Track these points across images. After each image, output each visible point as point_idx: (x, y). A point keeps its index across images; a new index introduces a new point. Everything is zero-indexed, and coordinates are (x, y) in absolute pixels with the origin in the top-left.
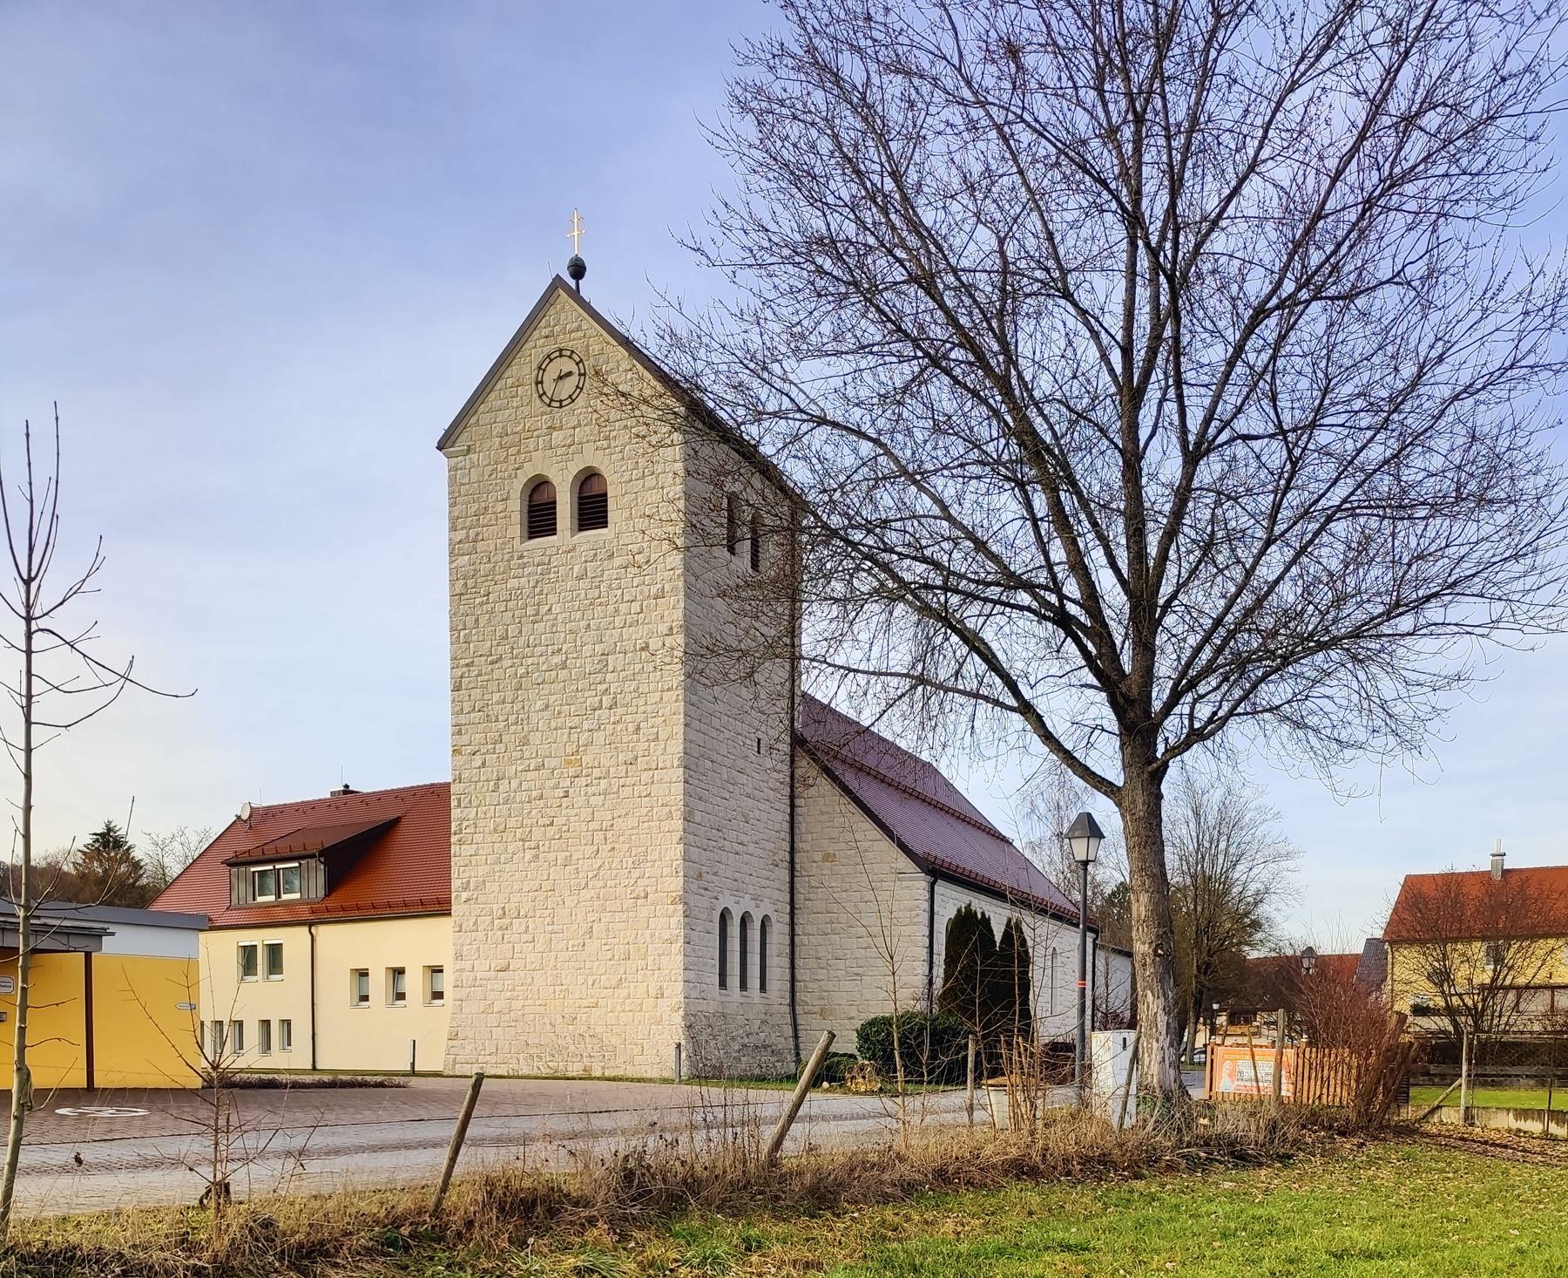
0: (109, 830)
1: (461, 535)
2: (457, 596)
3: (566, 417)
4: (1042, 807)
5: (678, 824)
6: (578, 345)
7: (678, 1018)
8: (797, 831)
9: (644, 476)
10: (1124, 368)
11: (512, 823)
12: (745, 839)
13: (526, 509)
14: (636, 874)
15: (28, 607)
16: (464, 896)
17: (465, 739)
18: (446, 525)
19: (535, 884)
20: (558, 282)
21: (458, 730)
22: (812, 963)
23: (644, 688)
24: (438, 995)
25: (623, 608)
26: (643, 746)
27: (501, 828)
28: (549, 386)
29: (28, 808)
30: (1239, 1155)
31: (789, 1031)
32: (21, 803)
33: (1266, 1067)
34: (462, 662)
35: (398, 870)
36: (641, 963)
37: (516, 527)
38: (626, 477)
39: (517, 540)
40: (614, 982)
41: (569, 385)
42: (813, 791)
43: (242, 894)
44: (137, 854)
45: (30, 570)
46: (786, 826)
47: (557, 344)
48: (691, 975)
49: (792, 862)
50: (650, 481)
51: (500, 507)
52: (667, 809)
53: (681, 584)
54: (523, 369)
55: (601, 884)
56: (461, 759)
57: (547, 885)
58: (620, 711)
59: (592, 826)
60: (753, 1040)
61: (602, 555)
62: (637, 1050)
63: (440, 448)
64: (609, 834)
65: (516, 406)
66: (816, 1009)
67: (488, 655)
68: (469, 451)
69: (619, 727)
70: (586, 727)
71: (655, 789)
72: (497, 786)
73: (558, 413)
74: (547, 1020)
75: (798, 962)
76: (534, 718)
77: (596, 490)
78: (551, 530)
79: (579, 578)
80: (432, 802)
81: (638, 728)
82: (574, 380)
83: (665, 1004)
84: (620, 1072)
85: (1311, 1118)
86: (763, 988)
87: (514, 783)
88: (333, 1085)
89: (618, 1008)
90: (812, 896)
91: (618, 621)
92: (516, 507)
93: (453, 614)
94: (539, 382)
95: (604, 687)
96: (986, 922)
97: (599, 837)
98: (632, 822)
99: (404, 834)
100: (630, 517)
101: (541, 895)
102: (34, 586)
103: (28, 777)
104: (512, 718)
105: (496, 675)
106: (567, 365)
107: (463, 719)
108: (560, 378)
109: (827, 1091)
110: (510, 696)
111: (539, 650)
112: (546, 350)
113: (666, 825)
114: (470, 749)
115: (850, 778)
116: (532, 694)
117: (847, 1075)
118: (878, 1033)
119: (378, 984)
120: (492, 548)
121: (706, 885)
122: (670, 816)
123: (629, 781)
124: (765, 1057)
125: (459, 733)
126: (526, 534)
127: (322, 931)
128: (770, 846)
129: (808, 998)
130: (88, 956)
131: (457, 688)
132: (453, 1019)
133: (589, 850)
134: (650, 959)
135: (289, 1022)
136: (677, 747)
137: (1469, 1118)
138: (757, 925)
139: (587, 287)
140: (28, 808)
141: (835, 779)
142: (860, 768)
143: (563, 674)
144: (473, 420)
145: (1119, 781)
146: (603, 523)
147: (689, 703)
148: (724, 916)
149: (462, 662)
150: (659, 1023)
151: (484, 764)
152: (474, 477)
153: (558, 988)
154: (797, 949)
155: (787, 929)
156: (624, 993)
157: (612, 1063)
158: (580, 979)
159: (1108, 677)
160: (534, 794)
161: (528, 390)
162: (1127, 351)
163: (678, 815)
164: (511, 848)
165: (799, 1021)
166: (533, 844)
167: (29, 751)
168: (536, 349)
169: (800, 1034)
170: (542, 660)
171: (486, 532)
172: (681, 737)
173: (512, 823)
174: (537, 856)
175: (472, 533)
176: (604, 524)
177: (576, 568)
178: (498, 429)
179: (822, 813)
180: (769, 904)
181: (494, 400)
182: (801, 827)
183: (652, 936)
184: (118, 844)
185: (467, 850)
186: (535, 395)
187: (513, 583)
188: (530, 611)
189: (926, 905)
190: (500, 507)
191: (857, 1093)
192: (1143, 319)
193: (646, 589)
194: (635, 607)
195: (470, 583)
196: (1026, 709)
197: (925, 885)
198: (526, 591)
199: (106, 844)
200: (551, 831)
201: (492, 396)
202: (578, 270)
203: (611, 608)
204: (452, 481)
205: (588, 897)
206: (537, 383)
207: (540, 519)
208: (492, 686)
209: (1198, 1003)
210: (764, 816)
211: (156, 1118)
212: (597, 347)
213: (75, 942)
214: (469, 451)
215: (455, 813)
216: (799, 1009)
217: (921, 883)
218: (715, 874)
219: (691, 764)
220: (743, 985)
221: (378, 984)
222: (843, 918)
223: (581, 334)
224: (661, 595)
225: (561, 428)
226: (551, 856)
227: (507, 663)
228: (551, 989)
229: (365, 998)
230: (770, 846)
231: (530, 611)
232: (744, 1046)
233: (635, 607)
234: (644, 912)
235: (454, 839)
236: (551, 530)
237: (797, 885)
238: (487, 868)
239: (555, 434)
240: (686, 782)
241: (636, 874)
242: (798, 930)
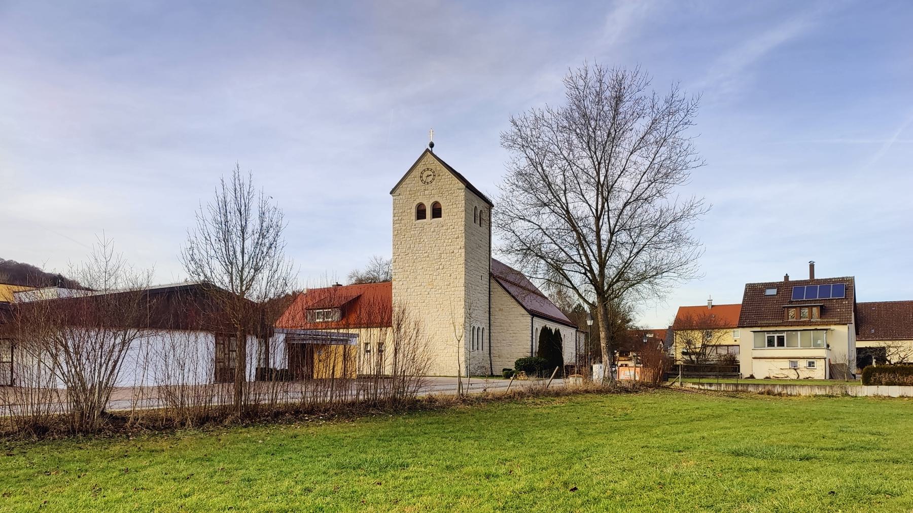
3: (429, 187)
10: (600, 271)
30: (626, 391)
33: (632, 373)
37: (414, 217)
41: (430, 178)
47: (429, 166)
54: (416, 173)
65: (414, 183)
78: (425, 218)
85: (642, 384)
92: (414, 211)
93: (394, 241)
96: (551, 330)
106: (430, 173)
115: (512, 290)
133: (436, 310)
137: (681, 385)
141: (501, 285)
142: (507, 281)
159: (593, 281)
161: (418, 179)
162: (597, 210)
168: (420, 167)
180: (484, 325)
182: (492, 301)
192: (600, 203)
202: (432, 145)
204: (394, 203)
207: (421, 213)
217: (529, 318)
224: (458, 238)
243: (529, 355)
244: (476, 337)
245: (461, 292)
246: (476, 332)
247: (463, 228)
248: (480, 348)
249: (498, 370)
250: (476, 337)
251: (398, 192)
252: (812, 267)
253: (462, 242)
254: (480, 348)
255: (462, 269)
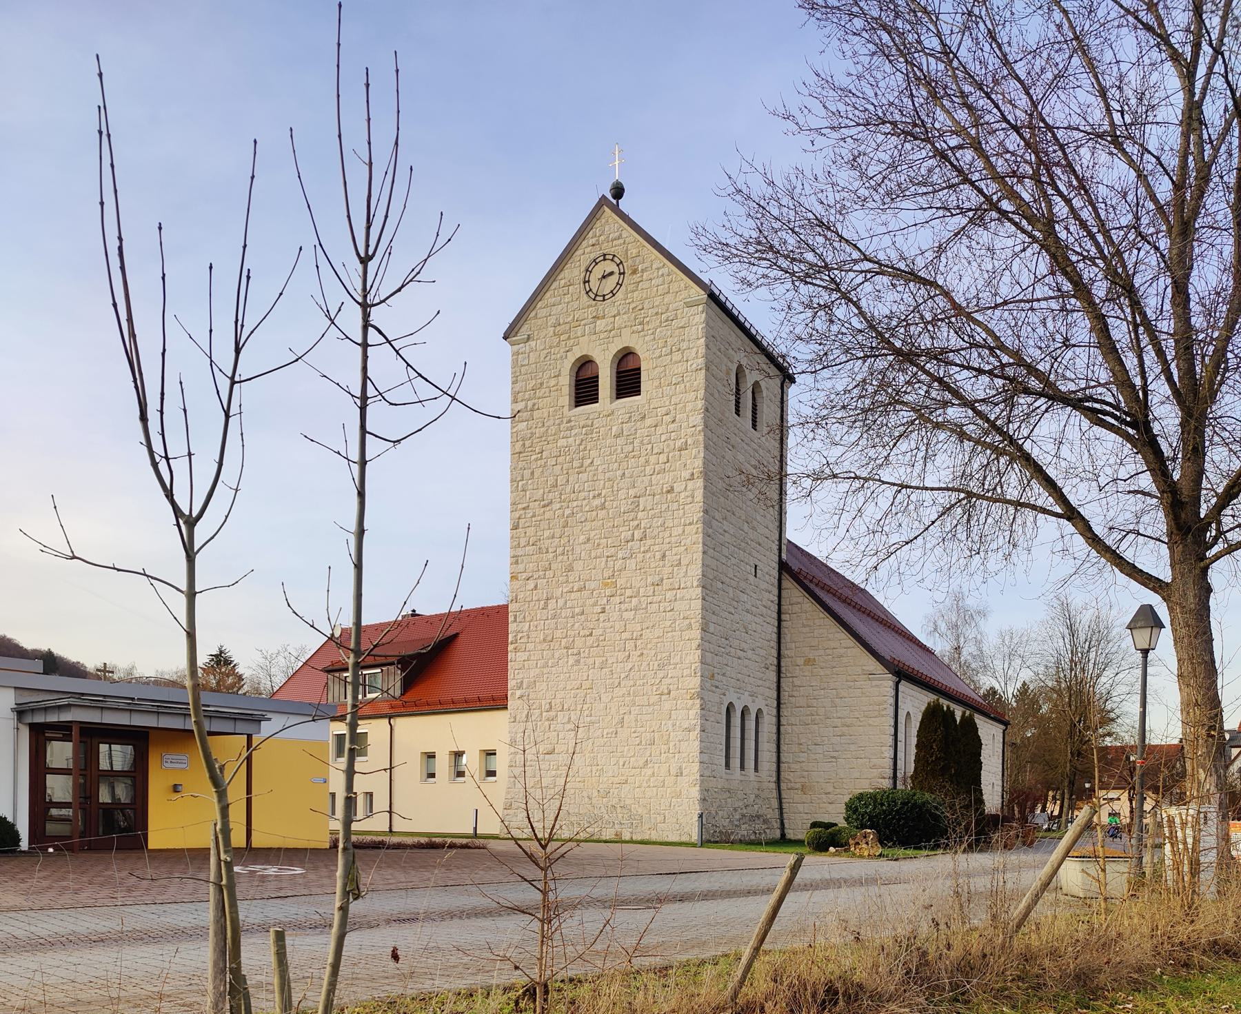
0: (221, 652)
2: (517, 454)
3: (609, 308)
4: (943, 627)
5: (696, 633)
6: (619, 251)
7: (695, 792)
8: (783, 641)
11: (558, 634)
12: (744, 645)
13: (573, 383)
14: (660, 674)
15: (365, 293)
16: (518, 693)
17: (521, 567)
18: (509, 398)
19: (576, 684)
20: (603, 201)
21: (516, 560)
22: (795, 748)
23: (669, 523)
24: (460, 774)
25: (653, 459)
26: (667, 570)
27: (549, 638)
28: (594, 284)
29: (361, 532)
31: (775, 804)
32: (353, 527)
34: (520, 506)
35: (459, 673)
38: (657, 353)
39: (566, 408)
40: (641, 763)
41: (611, 283)
42: (796, 608)
43: (336, 695)
44: (239, 670)
45: (367, 246)
46: (775, 636)
48: (706, 758)
49: (779, 666)
51: (553, 382)
53: (701, 438)
54: (573, 272)
55: (632, 683)
56: (517, 584)
57: (586, 684)
58: (649, 542)
59: (625, 636)
60: (749, 811)
61: (636, 417)
62: (660, 818)
63: (505, 338)
64: (639, 643)
65: (567, 301)
66: (798, 786)
67: (540, 500)
68: (528, 339)
69: (648, 555)
70: (620, 555)
72: (546, 605)
73: (601, 306)
75: (783, 747)
76: (578, 549)
77: (631, 366)
78: (595, 399)
79: (616, 437)
80: (491, 623)
81: (664, 556)
82: (616, 277)
83: (684, 781)
84: (646, 837)
86: (756, 769)
87: (561, 602)
88: (420, 846)
90: (795, 693)
91: (648, 470)
92: (566, 382)
93: (513, 469)
94: (586, 282)
95: (636, 523)
98: (658, 632)
99: (461, 649)
100: (660, 386)
101: (581, 693)
102: (372, 266)
103: (361, 494)
104: (560, 550)
105: (547, 515)
106: (610, 267)
107: (519, 552)
108: (604, 277)
109: (834, 855)
110: (558, 532)
111: (582, 495)
112: (593, 256)
114: (524, 576)
116: (577, 530)
117: (851, 842)
118: (866, 806)
119: (443, 765)
120: (546, 415)
121: (717, 683)
122: (690, 626)
123: (656, 599)
124: (759, 826)
126: (573, 403)
127: (399, 723)
128: (763, 653)
129: (791, 776)
130: (250, 737)
131: (515, 527)
132: (508, 793)
133: (621, 656)
134: (671, 744)
135: (371, 794)
136: (696, 571)
138: (753, 716)
139: (624, 204)
140: (361, 532)
143: (602, 514)
144: (533, 314)
145: (1165, 574)
146: (637, 391)
147: (707, 535)
148: (730, 709)
149: (520, 506)
150: (679, 796)
151: (536, 587)
152: (532, 360)
154: (782, 737)
155: (774, 720)
156: (650, 772)
157: (639, 829)
158: (613, 761)
160: (577, 610)
161: (578, 288)
163: (696, 626)
164: (557, 655)
165: (784, 795)
166: (575, 651)
167: (363, 463)
168: (584, 255)
169: (784, 806)
170: (584, 503)
171: (541, 403)
172: (699, 562)
173: (558, 634)
174: (578, 661)
175: (530, 404)
176: (638, 392)
177: (614, 429)
178: (552, 320)
179: (804, 626)
180: (763, 701)
181: (549, 298)
182: (786, 638)
184: (228, 662)
185: (522, 656)
187: (562, 442)
189: (892, 701)
190: (553, 382)
191: (861, 857)
193: (672, 443)
194: (663, 458)
195: (528, 443)
196: (1071, 514)
197: (891, 684)
198: (573, 448)
199: (218, 663)
200: (590, 640)
201: (548, 295)
202: (618, 191)
203: (642, 460)
204: (515, 364)
205: (621, 693)
206: (585, 282)
207: (585, 391)
208: (544, 525)
209: (1072, 783)
210: (759, 628)
211: (312, 876)
212: (635, 251)
213: (241, 727)
214: (528, 339)
215: (512, 627)
216: (783, 786)
217: (888, 681)
218: (724, 675)
219: (707, 585)
220: (742, 767)
221: (443, 765)
223: (621, 241)
225: (603, 317)
226: (591, 661)
227: (556, 506)
228: (589, 769)
229: (432, 775)
230: (763, 653)
232: (743, 816)
233: (663, 458)
234: (667, 706)
235: (510, 648)
236: (595, 399)
237: (783, 684)
238: (538, 671)
239: (598, 322)
240: (704, 599)
241: (660, 674)
242: (783, 721)
243: (887, 784)
244: (736, 732)
245: (691, 602)
246: (736, 720)
247: (698, 419)
248: (750, 763)
249: (799, 828)
250: (736, 732)
251: (524, 331)
253: (695, 460)
254: (750, 763)
255: (694, 536)
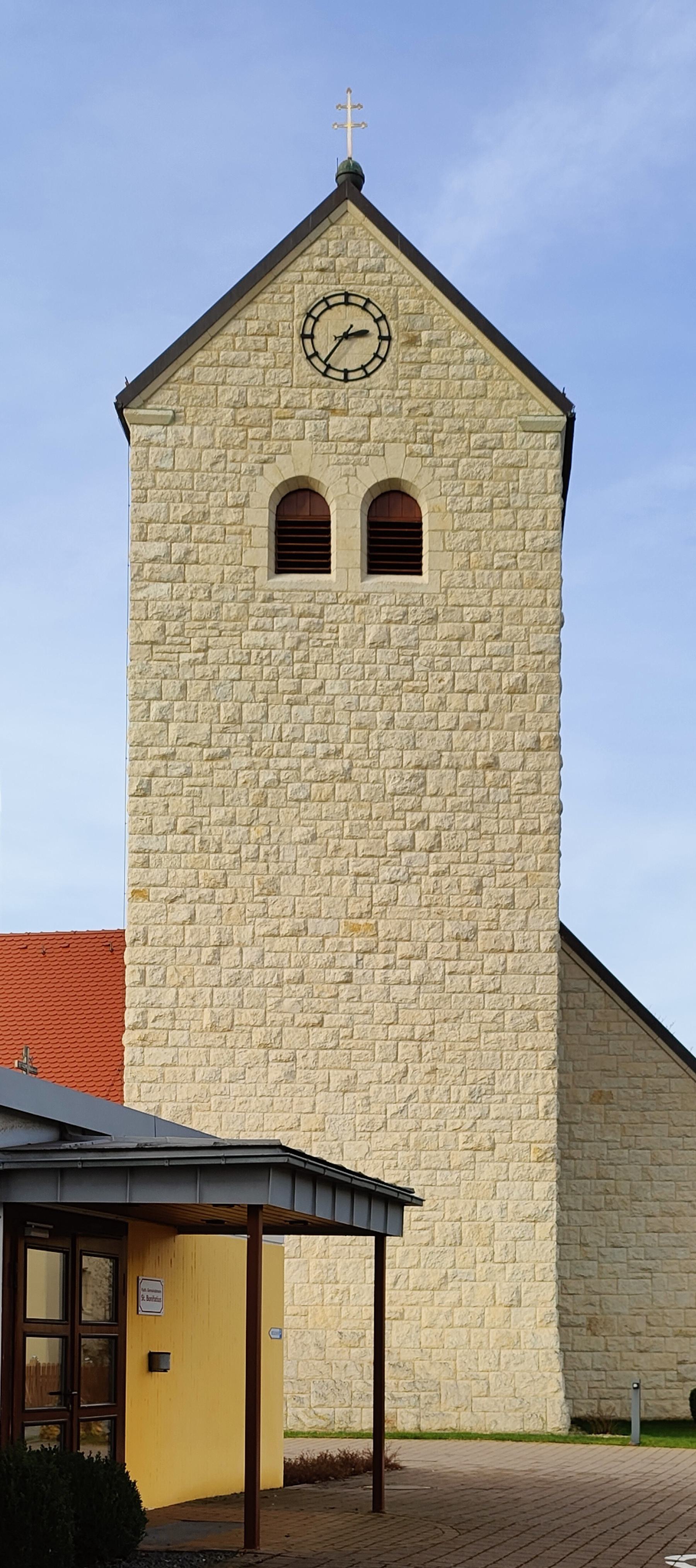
1: (157, 549)
6: (380, 295)
9: (491, 508)
14: (475, 1111)
17: (156, 874)
18: (125, 529)
21: (143, 859)
25: (454, 700)
26: (485, 914)
27: (225, 1023)
28: (324, 343)
34: (154, 751)
36: (481, 1252)
37: (260, 549)
38: (462, 503)
39: (262, 573)
40: (434, 1280)
41: (356, 354)
50: (502, 517)
52: (530, 1015)
55: (411, 1124)
58: (447, 856)
59: (395, 1031)
61: (420, 614)
64: (427, 1047)
65: (256, 358)
66: (582, 1320)
69: (446, 881)
71: (508, 982)
73: (341, 391)
74: (309, 1339)
76: (288, 854)
81: (480, 887)
82: (370, 344)
87: (250, 955)
89: (442, 1321)
91: (444, 719)
92: (261, 520)
95: (419, 816)
97: (406, 1050)
98: (465, 1030)
105: (219, 777)
106: (362, 321)
107: (152, 842)
108: (346, 336)
111: (299, 748)
112: (321, 291)
113: (528, 1040)
114: (165, 893)
116: (287, 815)
120: (215, 577)
125: (146, 864)
133: (389, 1070)
134: (498, 1247)
143: (344, 790)
144: (184, 372)
146: (410, 563)
149: (154, 751)
150: (516, 1344)
151: (192, 919)
153: (329, 1289)
156: (451, 1297)
160: (288, 973)
168: (301, 283)
170: (304, 764)
173: (245, 1016)
174: (292, 1074)
175: (178, 550)
178: (229, 394)
181: (221, 346)
183: (503, 1209)
185: (156, 1055)
186: (299, 355)
187: (250, 638)
188: (284, 684)
190: (231, 516)
193: (494, 677)
194: (475, 701)
195: (172, 627)
200: (319, 1036)
201: (219, 342)
203: (431, 699)
205: (389, 1143)
206: (303, 336)
207: (300, 539)
212: (413, 303)
214: (174, 420)
222: (624, 1187)
223: (380, 277)
225: (345, 412)
226: (320, 1076)
227: (239, 761)
231: (284, 684)
233: (475, 701)
234: (488, 1171)
241: (475, 1111)
251: (163, 401)
252: (51, 1394)
